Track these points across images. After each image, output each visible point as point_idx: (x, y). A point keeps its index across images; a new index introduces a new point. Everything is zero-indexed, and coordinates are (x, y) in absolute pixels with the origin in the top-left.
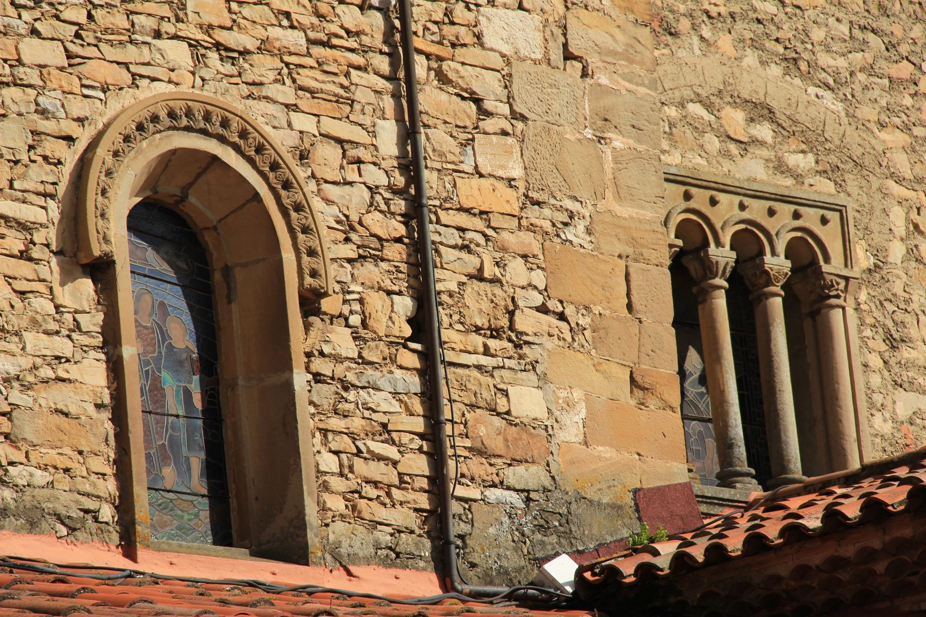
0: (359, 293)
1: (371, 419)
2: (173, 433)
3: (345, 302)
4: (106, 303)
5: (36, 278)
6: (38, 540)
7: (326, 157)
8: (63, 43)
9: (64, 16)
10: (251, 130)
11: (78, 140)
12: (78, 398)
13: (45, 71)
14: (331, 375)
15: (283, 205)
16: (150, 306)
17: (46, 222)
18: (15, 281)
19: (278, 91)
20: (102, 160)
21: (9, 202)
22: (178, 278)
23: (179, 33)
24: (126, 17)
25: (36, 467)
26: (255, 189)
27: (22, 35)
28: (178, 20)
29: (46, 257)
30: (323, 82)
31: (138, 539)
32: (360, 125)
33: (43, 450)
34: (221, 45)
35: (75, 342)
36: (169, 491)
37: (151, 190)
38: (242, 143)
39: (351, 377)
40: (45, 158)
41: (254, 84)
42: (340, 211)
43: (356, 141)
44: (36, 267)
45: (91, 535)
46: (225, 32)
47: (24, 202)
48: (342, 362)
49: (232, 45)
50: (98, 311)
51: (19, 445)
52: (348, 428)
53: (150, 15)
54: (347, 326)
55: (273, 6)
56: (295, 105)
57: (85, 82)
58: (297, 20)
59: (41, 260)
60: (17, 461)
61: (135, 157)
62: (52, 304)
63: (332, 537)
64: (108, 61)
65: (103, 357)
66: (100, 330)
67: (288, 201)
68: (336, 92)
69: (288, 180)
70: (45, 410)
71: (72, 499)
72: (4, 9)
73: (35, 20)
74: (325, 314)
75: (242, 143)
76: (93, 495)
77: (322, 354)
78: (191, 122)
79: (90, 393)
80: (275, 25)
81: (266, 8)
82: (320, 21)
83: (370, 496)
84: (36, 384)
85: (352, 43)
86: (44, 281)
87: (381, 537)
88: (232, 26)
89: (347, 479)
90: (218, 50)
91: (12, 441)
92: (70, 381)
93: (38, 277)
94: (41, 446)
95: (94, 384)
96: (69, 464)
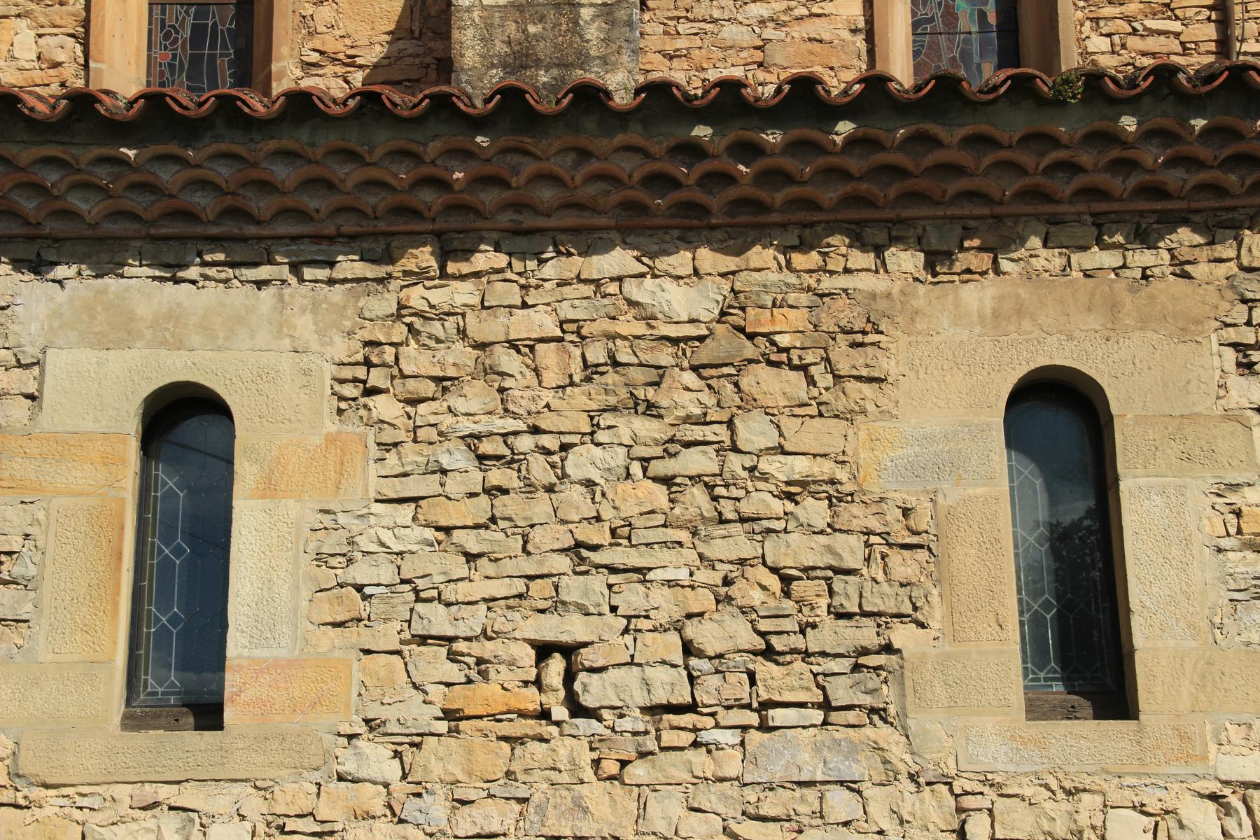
89: (1119, 55)
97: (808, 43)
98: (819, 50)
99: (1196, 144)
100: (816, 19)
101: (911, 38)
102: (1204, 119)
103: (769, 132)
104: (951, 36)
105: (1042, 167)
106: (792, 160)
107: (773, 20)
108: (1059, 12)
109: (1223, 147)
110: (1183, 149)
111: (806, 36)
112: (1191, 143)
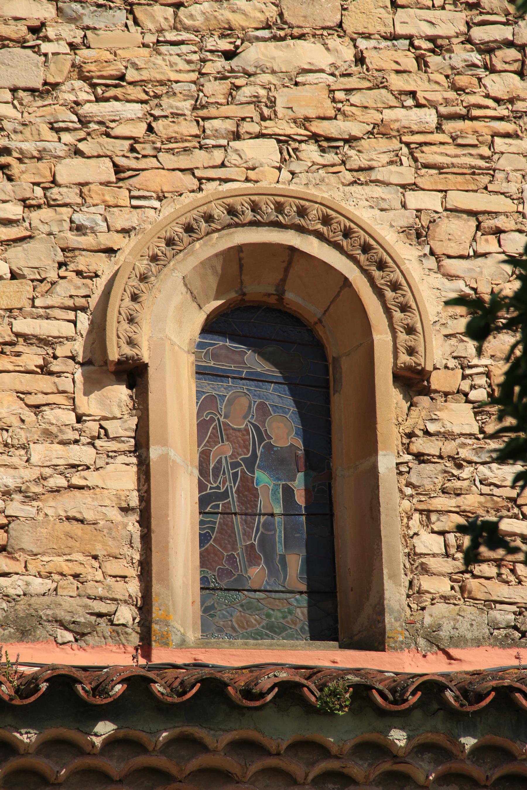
0: (486, 366)
1: (493, 495)
2: (264, 532)
3: (464, 377)
4: (141, 407)
5: (56, 391)
6: (29, 648)
7: (451, 232)
8: (111, 158)
9: (113, 133)
10: (334, 214)
11: (121, 251)
12: (96, 503)
13: (85, 189)
14: (438, 454)
15: (377, 286)
16: (247, 408)
17: (73, 335)
18: (29, 396)
19: (391, 172)
20: (132, 266)
21: (29, 320)
22: (284, 378)
23: (264, 131)
24: (195, 123)
25: (35, 576)
26: (342, 274)
27: (60, 157)
28: (263, 118)
29: (70, 369)
30: (456, 156)
31: (154, 638)
32: (502, 194)
33: (46, 558)
34: (320, 136)
35: (99, 448)
36: (255, 591)
37: (236, 292)
38: (324, 229)
39: (464, 453)
40: (79, 273)
41: (360, 169)
42: (466, 285)
43: (494, 210)
44: (56, 380)
45: (105, 638)
46: (326, 123)
47: (47, 318)
48: (454, 440)
49: (335, 135)
50: (132, 416)
51: (16, 555)
52: (459, 507)
53: (227, 118)
54: (468, 401)
55: (393, 88)
56: (415, 184)
57: (135, 193)
58: (424, 98)
59: (63, 373)
60: (11, 571)
61: (184, 259)
62: (74, 414)
63: (428, 621)
64: (168, 170)
65: (134, 460)
66: (133, 434)
67: (382, 281)
68: (473, 164)
69: (381, 260)
70: (52, 519)
71: (80, 604)
72: (39, 135)
73: (80, 140)
74: (436, 391)
75: (324, 229)
76: (107, 599)
77: (427, 433)
78: (259, 217)
79: (113, 498)
80: (396, 107)
81: (383, 91)
82: (458, 94)
83: (487, 575)
84: (43, 494)
85: (502, 111)
86: (64, 392)
87: (498, 616)
88: (336, 115)
89: (454, 559)
90: (317, 141)
91: (9, 553)
92: (89, 487)
93: (58, 390)
94: (43, 554)
95: (118, 488)
96: (78, 569)
97: (66, 523)
98: (79, 533)
99: (468, 762)
100: (76, 492)
101: (197, 518)
102: (474, 737)
103: (23, 731)
104: (249, 518)
105: (311, 777)
106: (46, 761)
107: (20, 492)
108: (381, 500)
109: (495, 767)
110: (454, 766)
111: (63, 514)
112: (462, 761)
